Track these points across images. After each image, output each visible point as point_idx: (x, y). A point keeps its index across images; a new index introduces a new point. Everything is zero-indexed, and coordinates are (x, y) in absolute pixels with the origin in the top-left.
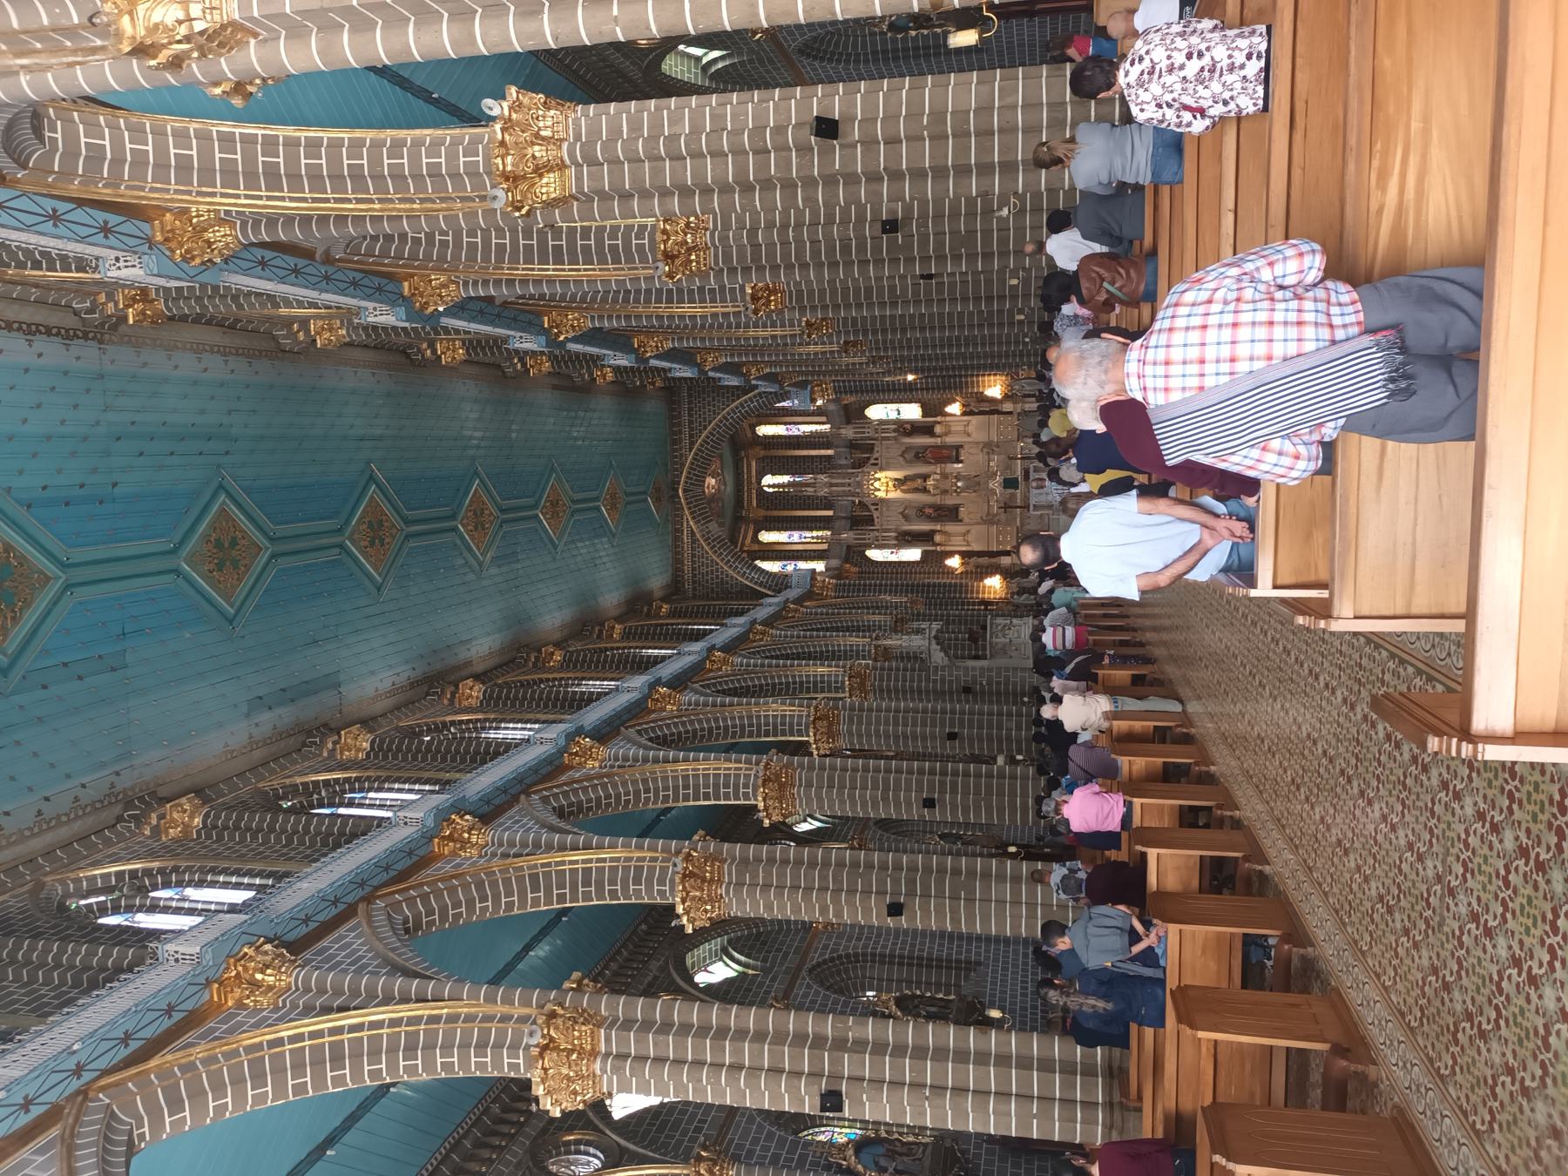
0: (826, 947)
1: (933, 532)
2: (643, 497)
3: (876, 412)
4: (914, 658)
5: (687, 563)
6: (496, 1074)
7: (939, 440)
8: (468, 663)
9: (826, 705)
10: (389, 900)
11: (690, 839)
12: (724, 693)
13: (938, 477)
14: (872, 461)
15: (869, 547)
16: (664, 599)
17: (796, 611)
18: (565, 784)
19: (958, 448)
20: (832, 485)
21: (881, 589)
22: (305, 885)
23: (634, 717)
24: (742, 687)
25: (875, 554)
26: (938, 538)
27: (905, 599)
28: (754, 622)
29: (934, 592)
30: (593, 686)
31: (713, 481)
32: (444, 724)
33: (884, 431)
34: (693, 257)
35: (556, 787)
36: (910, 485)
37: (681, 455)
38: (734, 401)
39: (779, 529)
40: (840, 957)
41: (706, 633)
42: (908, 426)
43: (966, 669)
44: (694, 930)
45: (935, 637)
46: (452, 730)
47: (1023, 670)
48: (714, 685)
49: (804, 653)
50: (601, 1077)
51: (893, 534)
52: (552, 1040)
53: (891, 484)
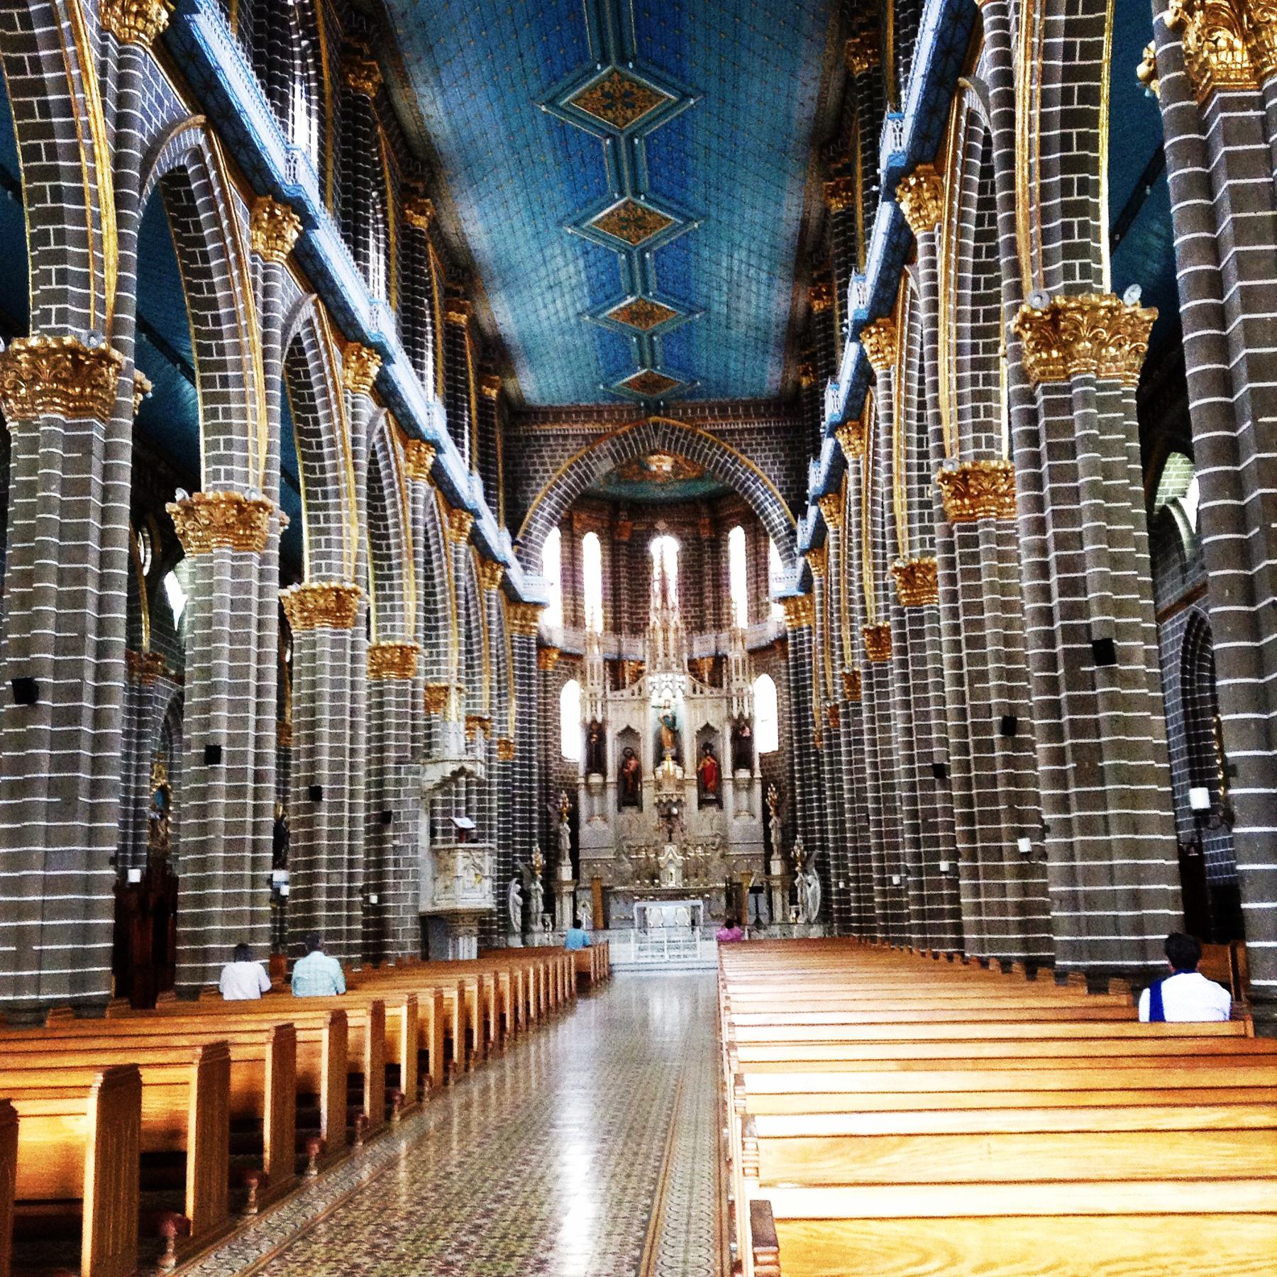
1: (604, 774)
2: (648, 363)
4: (425, 747)
5: (553, 429)
8: (405, 80)
9: (360, 608)
10: (205, 149)
12: (373, 462)
14: (698, 686)
16: (503, 393)
17: (493, 579)
19: (719, 803)
21: (525, 700)
24: (381, 489)
26: (596, 779)
27: (511, 733)
28: (476, 514)
29: (522, 773)
30: (377, 261)
31: (667, 467)
33: (741, 701)
34: (1055, 354)
35: (219, 176)
36: (667, 737)
37: (705, 419)
38: (781, 490)
41: (459, 444)
42: (747, 734)
46: (304, 43)
48: (384, 448)
49: (434, 586)
53: (668, 712)
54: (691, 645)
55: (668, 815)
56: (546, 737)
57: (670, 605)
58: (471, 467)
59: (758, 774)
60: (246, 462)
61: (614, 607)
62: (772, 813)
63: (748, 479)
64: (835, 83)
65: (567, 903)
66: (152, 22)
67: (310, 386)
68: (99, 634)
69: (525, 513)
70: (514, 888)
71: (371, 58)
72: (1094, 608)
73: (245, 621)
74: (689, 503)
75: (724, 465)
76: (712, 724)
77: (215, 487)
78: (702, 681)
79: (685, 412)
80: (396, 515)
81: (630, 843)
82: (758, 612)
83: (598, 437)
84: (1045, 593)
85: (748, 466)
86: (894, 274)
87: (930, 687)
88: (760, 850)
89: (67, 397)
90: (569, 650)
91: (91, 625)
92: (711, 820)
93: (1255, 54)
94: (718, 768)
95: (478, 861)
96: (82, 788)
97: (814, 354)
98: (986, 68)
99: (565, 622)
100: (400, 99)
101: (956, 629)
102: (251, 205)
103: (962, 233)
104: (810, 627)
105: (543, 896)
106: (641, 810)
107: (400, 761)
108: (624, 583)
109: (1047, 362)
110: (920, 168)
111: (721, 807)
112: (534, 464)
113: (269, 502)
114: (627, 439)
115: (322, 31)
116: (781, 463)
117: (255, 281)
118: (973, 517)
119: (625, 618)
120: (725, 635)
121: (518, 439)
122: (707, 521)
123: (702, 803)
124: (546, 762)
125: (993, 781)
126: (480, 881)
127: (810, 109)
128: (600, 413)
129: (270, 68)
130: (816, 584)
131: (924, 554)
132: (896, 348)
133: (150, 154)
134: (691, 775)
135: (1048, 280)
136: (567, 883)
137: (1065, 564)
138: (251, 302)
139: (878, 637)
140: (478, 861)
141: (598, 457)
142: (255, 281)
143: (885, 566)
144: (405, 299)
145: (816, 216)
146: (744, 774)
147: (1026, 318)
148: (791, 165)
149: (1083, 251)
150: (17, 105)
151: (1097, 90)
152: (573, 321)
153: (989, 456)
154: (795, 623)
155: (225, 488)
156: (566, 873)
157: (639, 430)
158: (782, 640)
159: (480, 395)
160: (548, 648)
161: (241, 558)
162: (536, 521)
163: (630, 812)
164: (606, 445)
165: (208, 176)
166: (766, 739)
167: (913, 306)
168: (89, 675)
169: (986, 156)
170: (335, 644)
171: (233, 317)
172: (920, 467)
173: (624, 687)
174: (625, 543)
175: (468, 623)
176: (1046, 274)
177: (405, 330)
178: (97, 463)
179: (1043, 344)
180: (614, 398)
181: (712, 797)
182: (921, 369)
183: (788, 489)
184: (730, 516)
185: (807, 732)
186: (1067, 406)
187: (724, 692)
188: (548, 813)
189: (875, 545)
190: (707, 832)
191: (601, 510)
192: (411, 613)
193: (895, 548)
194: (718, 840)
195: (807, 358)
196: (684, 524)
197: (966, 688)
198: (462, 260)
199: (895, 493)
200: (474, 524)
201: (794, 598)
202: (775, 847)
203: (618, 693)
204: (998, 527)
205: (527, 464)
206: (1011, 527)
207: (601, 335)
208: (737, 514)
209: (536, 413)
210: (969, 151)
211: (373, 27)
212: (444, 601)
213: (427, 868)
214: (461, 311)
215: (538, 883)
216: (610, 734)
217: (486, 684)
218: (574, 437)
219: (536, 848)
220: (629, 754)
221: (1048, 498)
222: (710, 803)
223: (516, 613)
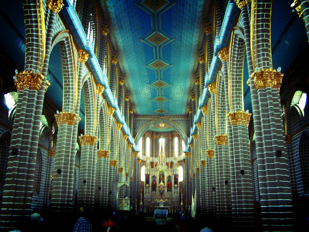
0: (44, 152)
1: (149, 185)
6: (26, 62)
10: (69, 38)
11: (79, 116)
12: (101, 111)
13: (163, 185)
16: (129, 100)
18: (93, 84)
19: (171, 191)
20: (162, 157)
22: (75, 17)
23: (107, 103)
26: (147, 185)
28: (122, 124)
30: (105, 70)
32: (108, 54)
40: (41, 156)
41: (120, 109)
43: (116, 192)
44: (55, 117)
46: (106, 56)
50: (23, 90)
51: (149, 174)
52: (34, 77)
54: (167, 160)
58: (122, 114)
59: (179, 185)
60: (93, 130)
61: (152, 152)
64: (202, 38)
66: (58, 7)
67: (88, 93)
68: (71, 162)
69: (136, 134)
71: (107, 28)
72: (241, 164)
73: (91, 158)
77: (87, 134)
78: (169, 167)
80: (115, 136)
83: (151, 120)
84: (233, 161)
86: (207, 99)
88: (179, 200)
89: (68, 122)
90: (143, 160)
91: (70, 160)
92: (169, 194)
93: (264, 84)
94: (171, 184)
96: (67, 188)
97: (192, 107)
98: (223, 69)
99: (142, 154)
100: (120, 64)
101: (217, 164)
102: (78, 51)
103: (219, 95)
104: (190, 158)
106: (156, 191)
107: (113, 182)
108: (154, 147)
109: (233, 122)
110: (212, 83)
113: (96, 137)
115: (109, 54)
117: (78, 67)
118: (221, 144)
119: (154, 154)
120: (173, 158)
121: (136, 120)
122: (170, 136)
123: (168, 191)
125: (223, 192)
127: (192, 67)
129: (85, 25)
130: (191, 150)
131: (212, 149)
132: (207, 111)
133: (83, 80)
134: (166, 185)
135: (233, 108)
136: (142, 205)
137: (236, 157)
138: (95, 102)
139: (203, 162)
142: (96, 98)
143: (205, 151)
144: (119, 97)
146: (176, 185)
147: (230, 114)
148: (188, 76)
149: (239, 104)
150: (64, 74)
151: (241, 78)
152: (147, 100)
153: (224, 134)
155: (89, 134)
158: (184, 160)
159: (130, 112)
161: (91, 147)
163: (154, 192)
164: (152, 122)
165: (69, 44)
166: (181, 179)
167: (210, 107)
168: (69, 169)
169: (223, 83)
170: (104, 161)
171: (72, 75)
172: (211, 133)
175: (120, 147)
176: (233, 107)
177: (110, 84)
178: (72, 133)
179: (233, 119)
180: (154, 113)
181: (170, 190)
184: (175, 135)
186: (237, 129)
189: (203, 145)
190: (168, 196)
191: (150, 133)
192: (116, 154)
193: (207, 147)
195: (191, 108)
196: (166, 136)
197: (219, 175)
198: (128, 90)
199: (207, 137)
200: (128, 138)
203: (152, 169)
204: (225, 146)
206: (227, 146)
208: (176, 135)
210: (220, 82)
211: (108, 23)
214: (128, 98)
216: (150, 177)
218: (146, 120)
220: (154, 181)
221: (233, 145)
222: (169, 191)
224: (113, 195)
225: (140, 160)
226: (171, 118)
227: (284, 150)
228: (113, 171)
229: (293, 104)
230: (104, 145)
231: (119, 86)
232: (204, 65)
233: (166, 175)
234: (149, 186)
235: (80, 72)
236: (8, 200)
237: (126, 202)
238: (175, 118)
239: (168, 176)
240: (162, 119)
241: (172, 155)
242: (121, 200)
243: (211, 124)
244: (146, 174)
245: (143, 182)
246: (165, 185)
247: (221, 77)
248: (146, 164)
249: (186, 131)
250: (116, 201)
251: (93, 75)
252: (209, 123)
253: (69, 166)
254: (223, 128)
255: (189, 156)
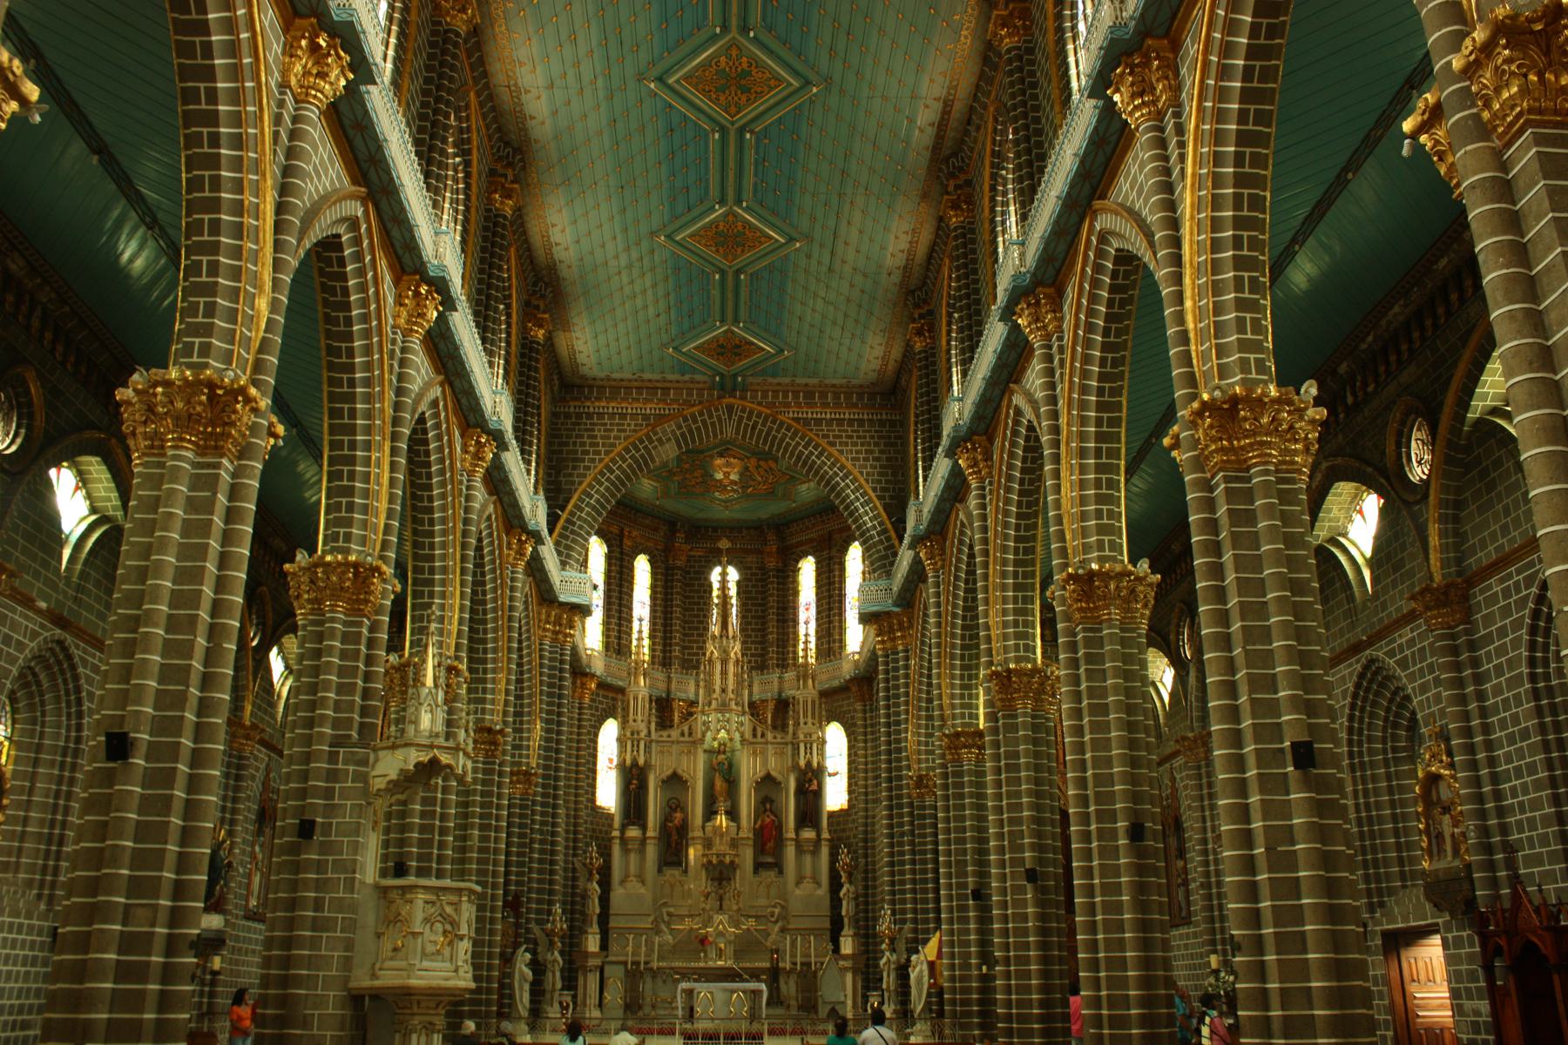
1: (644, 828)
3: (836, 739)
7: (792, 835)
15: (624, 725)
19: (778, 867)
20: (724, 662)
25: (609, 733)
26: (633, 832)
33: (808, 750)
38: (874, 490)
39: (653, 587)
42: (814, 787)
45: (434, 762)
47: (347, 963)
51: (641, 761)
55: (721, 873)
56: (577, 780)
57: (731, 633)
59: (825, 835)
62: (843, 880)
63: (836, 474)
64: (926, 236)
65: (593, 981)
70: (523, 958)
74: (756, 528)
75: (808, 457)
76: (774, 773)
78: (763, 722)
79: (765, 396)
81: (672, 910)
82: (830, 649)
83: (661, 418)
85: (837, 460)
87: (1272, 608)
94: (779, 828)
95: (449, 909)
102: (397, 282)
104: (906, 651)
105: (562, 971)
107: (337, 742)
108: (677, 612)
111: (781, 872)
112: (583, 444)
114: (695, 421)
116: (875, 459)
120: (790, 675)
121: (568, 416)
123: (758, 867)
124: (576, 810)
126: (451, 943)
127: (876, 364)
128: (666, 390)
129: (485, 320)
134: (746, 832)
136: (594, 955)
140: (449, 909)
141: (660, 440)
145: (958, 115)
146: (808, 834)
154: (888, 645)
156: (592, 943)
157: (710, 412)
160: (585, 675)
162: (582, 510)
163: (673, 873)
164: (670, 427)
173: (672, 726)
174: (679, 568)
181: (770, 860)
182: (930, 654)
183: (883, 489)
184: (801, 544)
185: (900, 778)
187: (789, 738)
188: (574, 870)
194: (777, 911)
196: (747, 552)
201: (888, 614)
202: (846, 920)
203: (665, 733)
205: (575, 444)
207: (677, 270)
208: (811, 540)
209: (591, 387)
212: (444, 545)
213: (369, 917)
215: (556, 953)
217: (502, 686)
219: (558, 908)
220: (674, 806)
223: (549, 616)
224: (326, 848)
225: (593, 676)
226: (788, 405)
227: (1153, 817)
228: (344, 655)
229: (1479, 406)
230: (483, 701)
231: (524, 346)
232: (934, 355)
233: (749, 769)
234: (643, 841)
235: (401, 377)
236: (248, 964)
237: (444, 917)
238: (811, 405)
239: (760, 773)
240: (730, 408)
241: (785, 659)
242: (394, 895)
243: (928, 692)
244: (628, 762)
245: (610, 817)
246: (739, 828)
247: (963, 524)
248: (626, 710)
249: (883, 489)
250: (353, 907)
251: (451, 385)
252: (920, 691)
253: (190, 716)
254: (970, 706)
255: (903, 637)
